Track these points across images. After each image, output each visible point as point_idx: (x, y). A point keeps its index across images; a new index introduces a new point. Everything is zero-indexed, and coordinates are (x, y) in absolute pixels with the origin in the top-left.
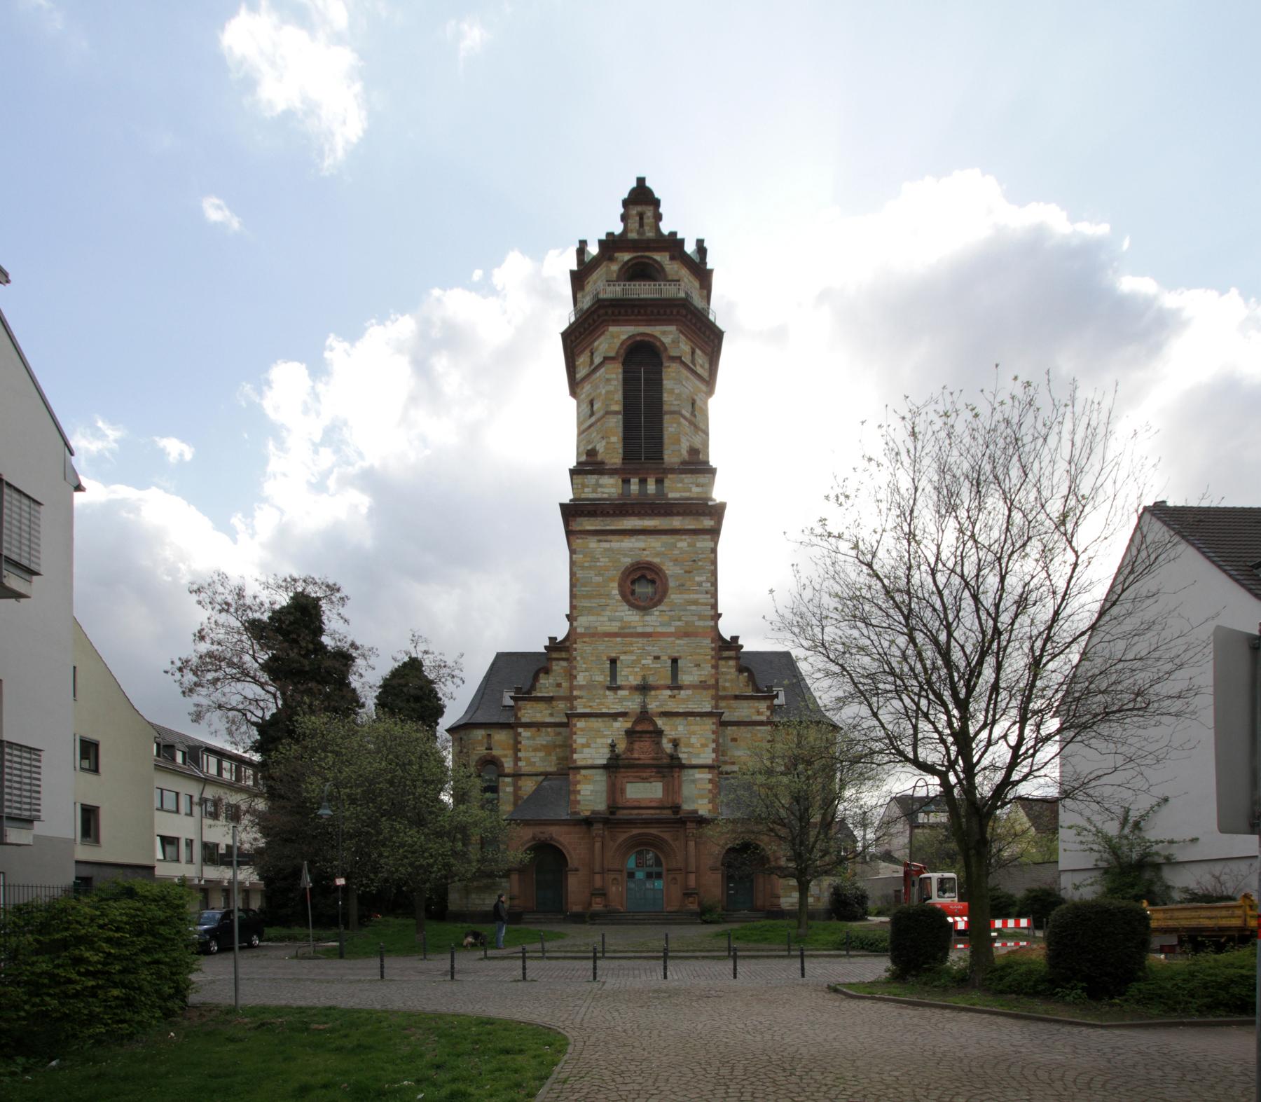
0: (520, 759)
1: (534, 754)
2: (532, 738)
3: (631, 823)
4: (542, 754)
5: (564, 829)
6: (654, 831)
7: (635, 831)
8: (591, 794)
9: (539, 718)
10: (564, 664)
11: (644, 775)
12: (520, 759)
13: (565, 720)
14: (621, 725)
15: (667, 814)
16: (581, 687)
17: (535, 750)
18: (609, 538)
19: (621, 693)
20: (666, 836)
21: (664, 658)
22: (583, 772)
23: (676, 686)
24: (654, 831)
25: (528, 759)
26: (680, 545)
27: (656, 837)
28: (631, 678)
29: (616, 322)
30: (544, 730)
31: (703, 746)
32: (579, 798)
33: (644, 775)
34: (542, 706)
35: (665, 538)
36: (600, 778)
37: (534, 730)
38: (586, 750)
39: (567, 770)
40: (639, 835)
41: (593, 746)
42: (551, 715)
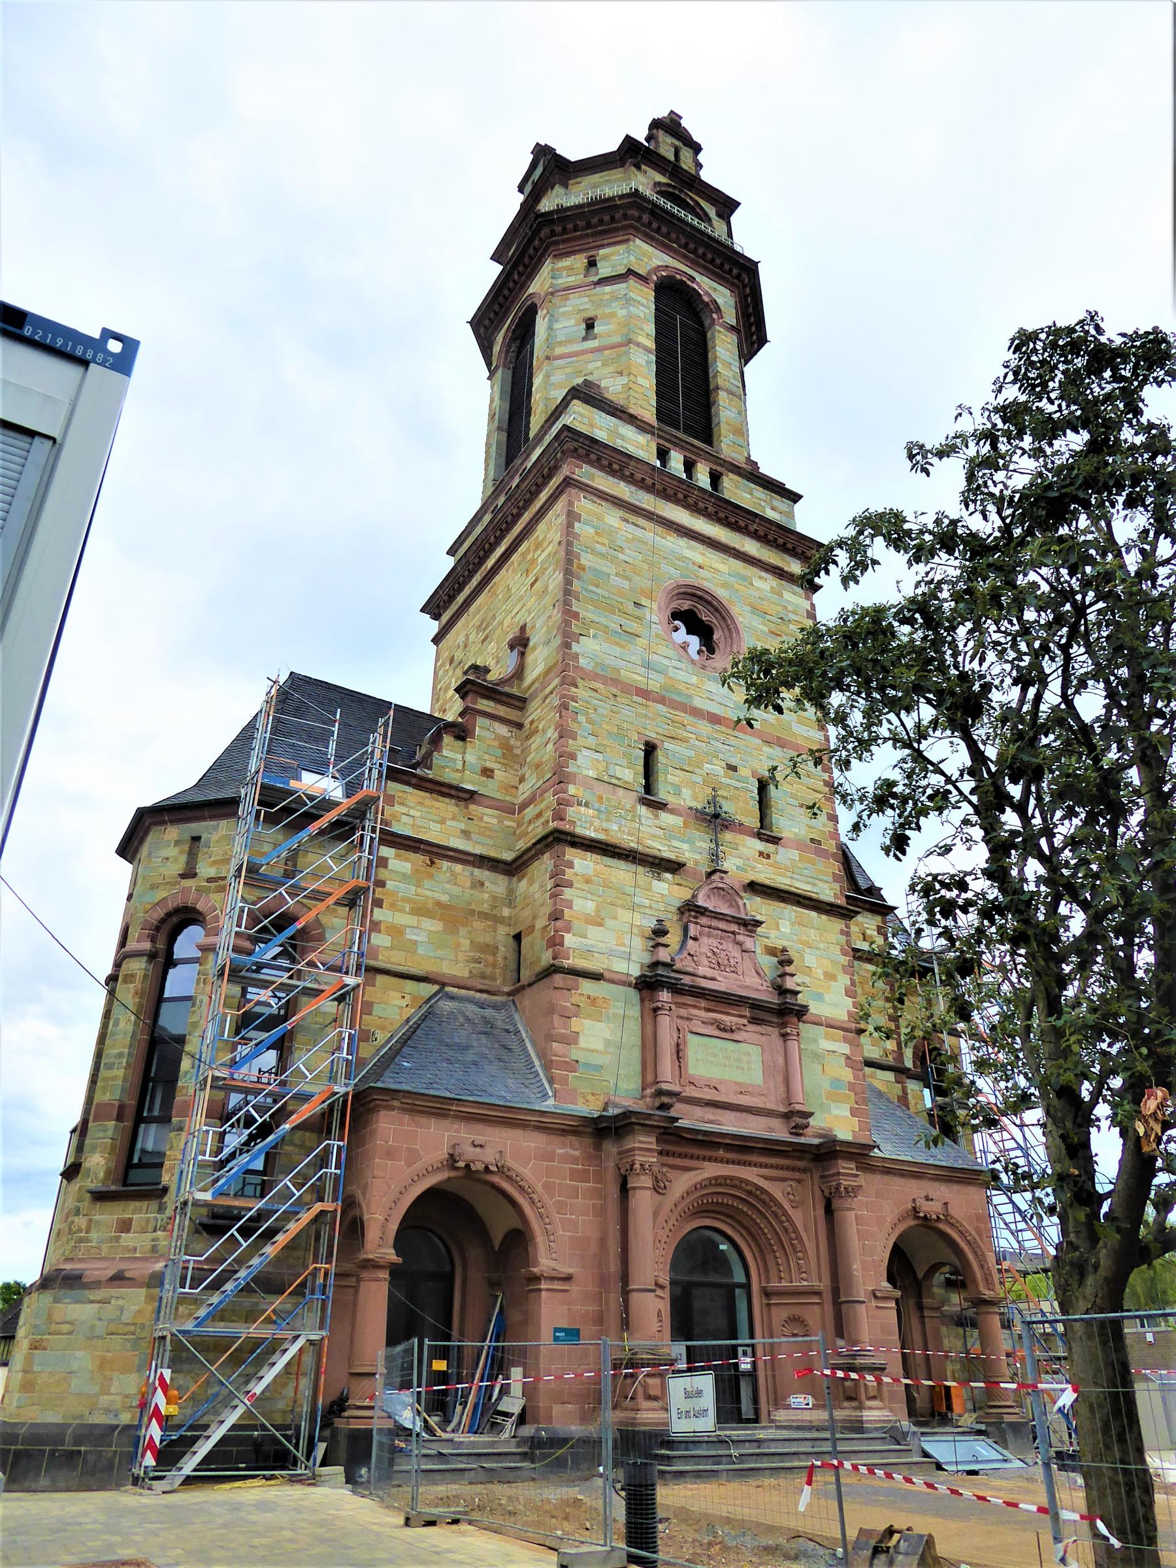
0: (376, 926)
1: (421, 923)
2: (416, 878)
3: (708, 1144)
4: (433, 925)
5: (534, 1142)
6: (750, 1174)
7: (712, 1170)
8: (601, 1051)
9: (433, 834)
10: (503, 730)
11: (728, 1020)
12: (376, 926)
13: (199, 954)
14: (667, 892)
15: (779, 1132)
16: (586, 783)
17: (420, 911)
18: (641, 521)
19: (664, 816)
20: (776, 1190)
21: (744, 772)
22: (586, 986)
23: (766, 833)
24: (750, 1174)
25: (396, 931)
26: (757, 583)
27: (756, 1192)
28: (686, 793)
29: (649, 238)
30: (445, 864)
31: (830, 977)
32: (575, 1054)
33: (728, 1020)
34: (447, 807)
35: (738, 565)
36: (624, 1005)
37: (420, 859)
38: (593, 932)
39: (533, 974)
40: (717, 1181)
41: (609, 922)
42: (466, 834)
